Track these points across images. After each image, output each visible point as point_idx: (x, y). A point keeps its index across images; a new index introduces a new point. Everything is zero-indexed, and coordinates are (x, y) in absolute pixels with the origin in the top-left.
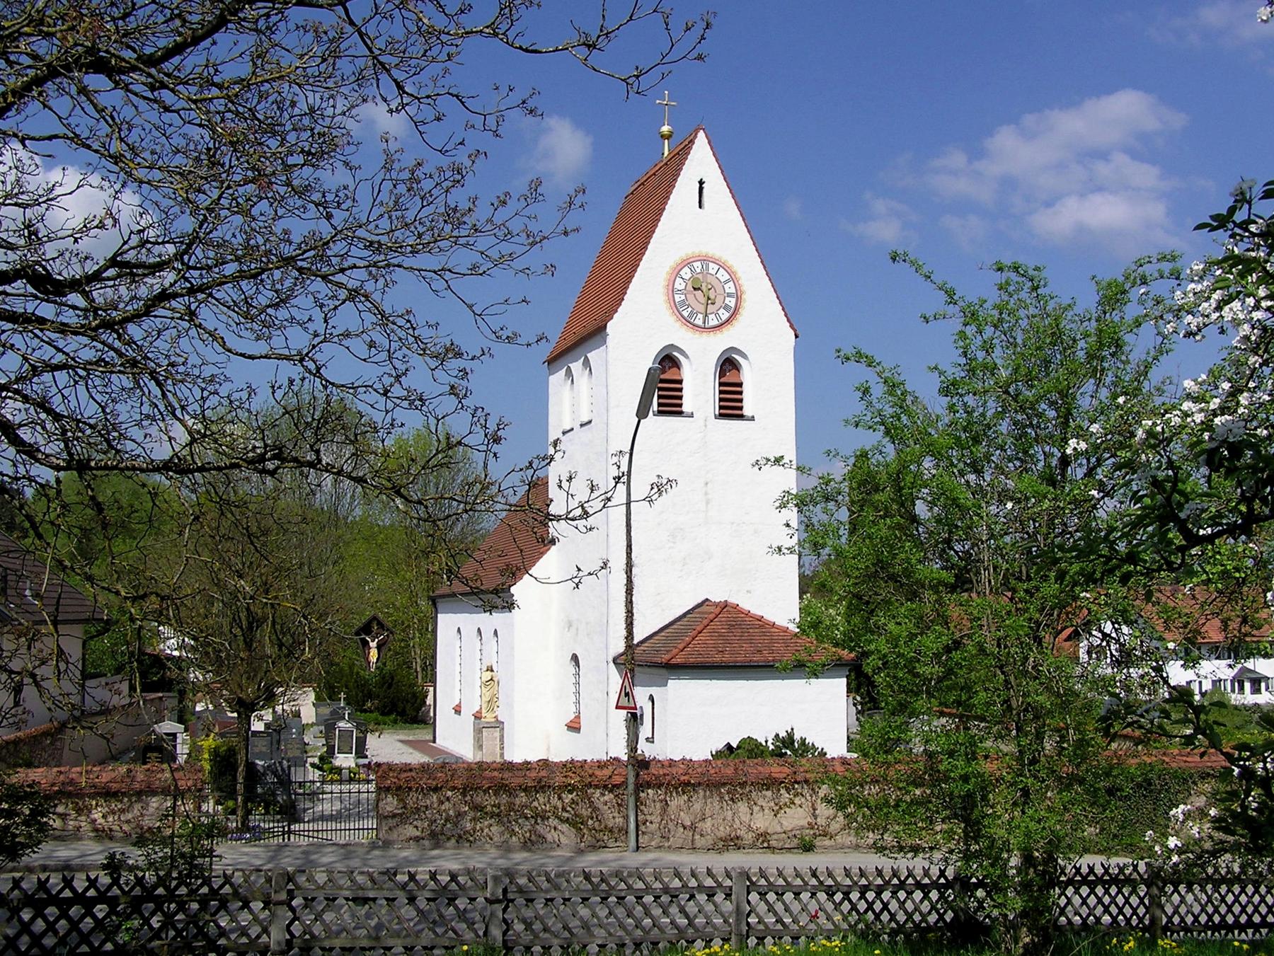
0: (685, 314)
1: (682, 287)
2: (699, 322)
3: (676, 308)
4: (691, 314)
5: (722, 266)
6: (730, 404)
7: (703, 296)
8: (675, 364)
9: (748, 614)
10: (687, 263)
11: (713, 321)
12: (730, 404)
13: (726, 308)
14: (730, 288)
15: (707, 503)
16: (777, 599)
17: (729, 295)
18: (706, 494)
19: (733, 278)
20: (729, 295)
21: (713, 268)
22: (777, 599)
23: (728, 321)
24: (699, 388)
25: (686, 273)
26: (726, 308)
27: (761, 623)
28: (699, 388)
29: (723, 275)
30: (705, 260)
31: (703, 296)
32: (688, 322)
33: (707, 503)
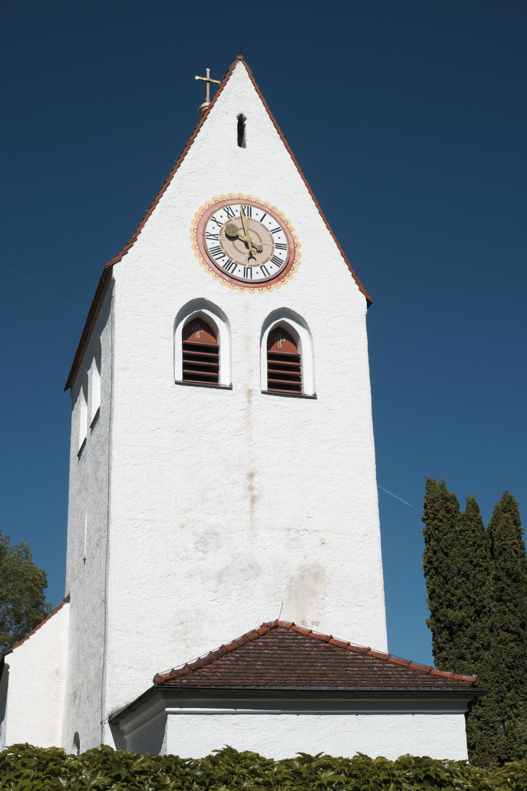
0: (221, 263)
1: (217, 230)
2: (239, 273)
3: (208, 256)
4: (229, 264)
5: (269, 211)
6: (284, 375)
7: (237, 241)
8: (292, 338)
9: (346, 647)
10: (224, 204)
11: (258, 275)
12: (284, 375)
13: (276, 260)
14: (280, 238)
15: (253, 500)
16: (357, 610)
17: (279, 246)
18: (251, 488)
19: (283, 226)
20: (279, 246)
21: (257, 214)
22: (357, 610)
23: (278, 277)
24: (242, 355)
25: (221, 216)
26: (276, 260)
27: (366, 652)
28: (242, 355)
29: (270, 223)
30: (248, 205)
31: (237, 241)
32: (224, 273)
33: (253, 500)
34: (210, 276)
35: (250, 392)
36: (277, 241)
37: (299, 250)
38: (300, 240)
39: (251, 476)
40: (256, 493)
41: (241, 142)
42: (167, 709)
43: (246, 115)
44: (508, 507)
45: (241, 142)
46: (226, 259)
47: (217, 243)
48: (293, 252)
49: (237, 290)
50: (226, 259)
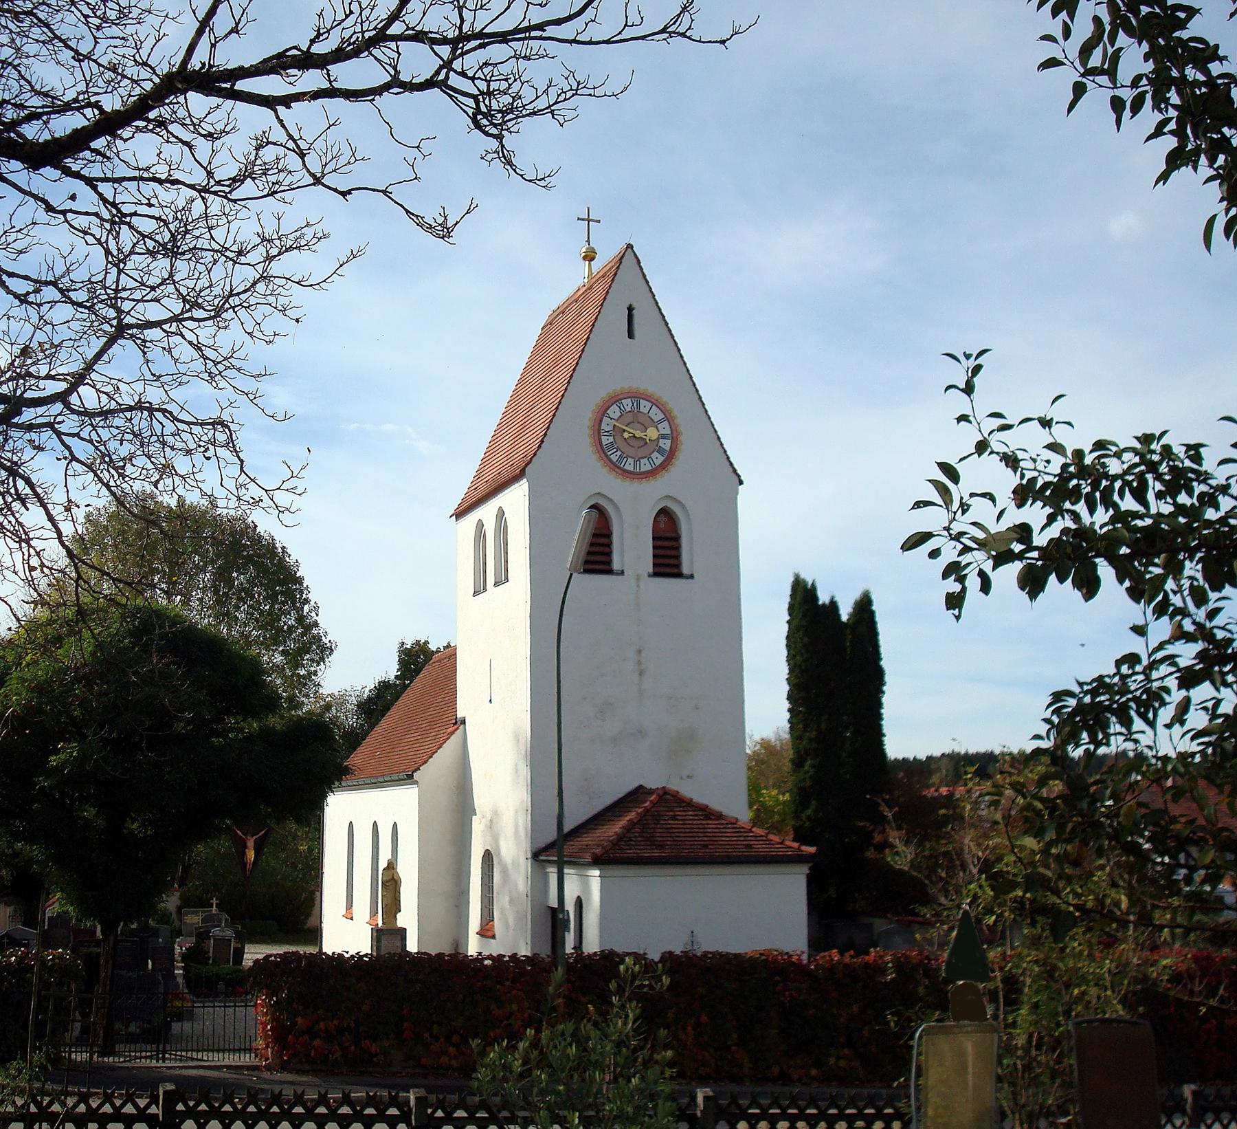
2: (629, 467)
5: (656, 403)
11: (645, 466)
18: (639, 663)
24: (633, 547)
26: (661, 451)
28: (633, 547)
34: (605, 471)
35: (638, 578)
36: (661, 444)
37: (682, 438)
38: (682, 429)
39: (640, 652)
40: (643, 667)
41: (631, 335)
42: (569, 948)
43: (634, 305)
44: (864, 606)
45: (631, 335)
46: (619, 453)
47: (611, 439)
48: (674, 437)
49: (627, 483)
50: (619, 453)
